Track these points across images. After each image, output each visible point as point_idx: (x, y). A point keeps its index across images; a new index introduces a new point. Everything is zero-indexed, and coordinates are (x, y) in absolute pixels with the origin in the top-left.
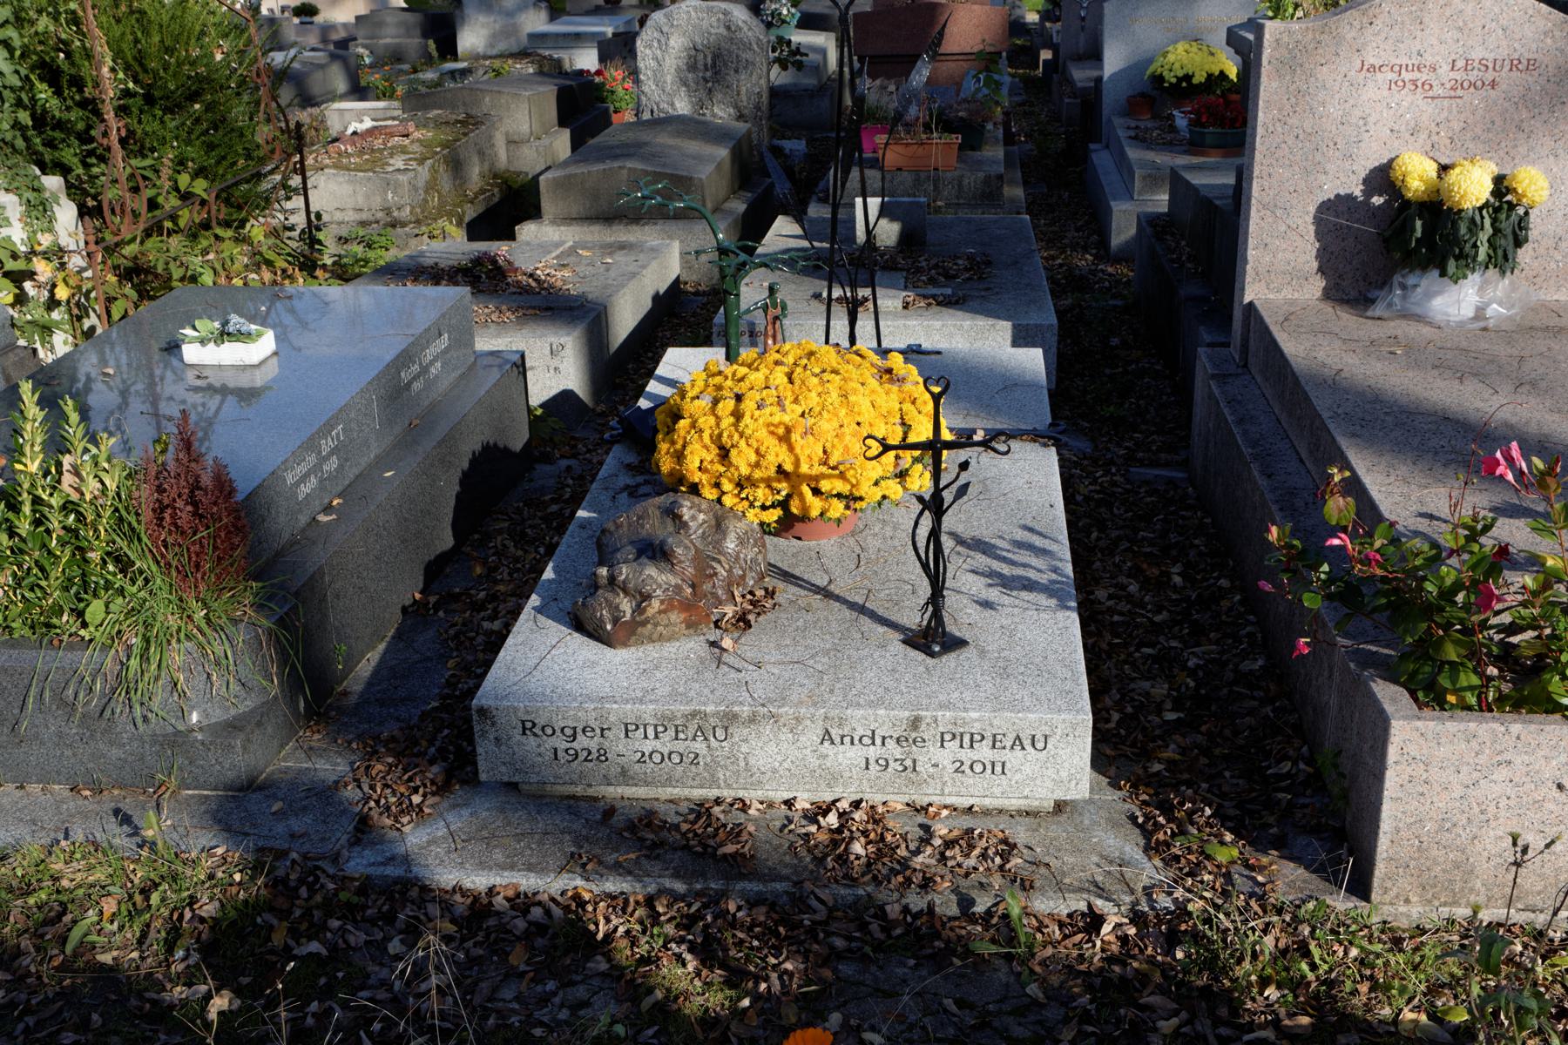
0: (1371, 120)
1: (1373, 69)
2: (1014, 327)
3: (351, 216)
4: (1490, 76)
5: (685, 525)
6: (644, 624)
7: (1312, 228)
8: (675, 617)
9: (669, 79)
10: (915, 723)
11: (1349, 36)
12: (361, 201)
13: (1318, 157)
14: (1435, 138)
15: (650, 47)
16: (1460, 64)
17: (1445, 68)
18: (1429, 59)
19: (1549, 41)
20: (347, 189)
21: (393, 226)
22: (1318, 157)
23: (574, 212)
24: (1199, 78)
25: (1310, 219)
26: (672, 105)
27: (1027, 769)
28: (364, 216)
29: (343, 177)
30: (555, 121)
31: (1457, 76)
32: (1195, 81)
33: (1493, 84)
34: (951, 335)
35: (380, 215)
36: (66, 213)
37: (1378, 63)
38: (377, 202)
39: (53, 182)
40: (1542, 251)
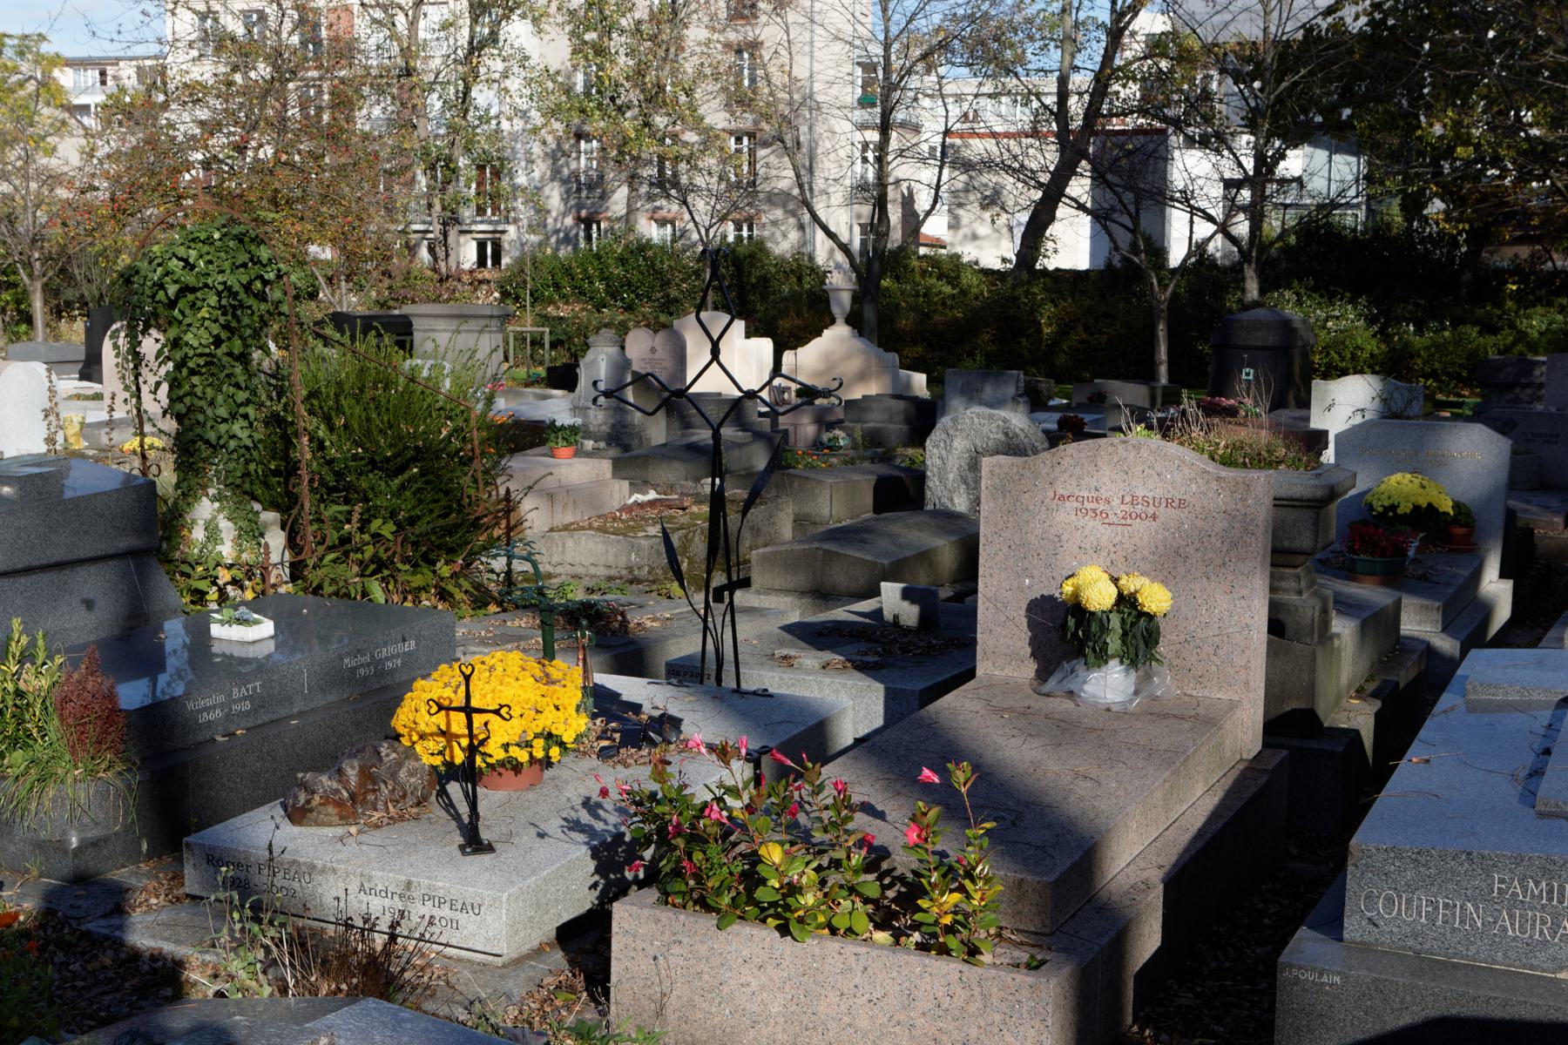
0: (1064, 538)
1: (1062, 498)
2: (887, 689)
3: (602, 571)
4: (1151, 510)
5: (381, 759)
6: (311, 811)
7: (1025, 621)
8: (331, 809)
9: (951, 476)
10: (409, 884)
11: (1044, 471)
12: (611, 560)
13: (1026, 563)
14: (1113, 556)
15: (938, 447)
16: (1128, 499)
17: (1116, 502)
18: (1103, 494)
19: (1194, 486)
20: (601, 548)
21: (631, 582)
22: (1026, 563)
23: (791, 586)
24: (1405, 509)
25: (1023, 612)
26: (951, 500)
27: (471, 927)
28: (612, 572)
29: (600, 537)
30: (871, 507)
31: (1128, 508)
32: (1400, 511)
33: (1154, 517)
34: (837, 691)
35: (624, 572)
36: (276, 540)
37: (1066, 494)
38: (622, 561)
39: (270, 516)
40: (1203, 656)
